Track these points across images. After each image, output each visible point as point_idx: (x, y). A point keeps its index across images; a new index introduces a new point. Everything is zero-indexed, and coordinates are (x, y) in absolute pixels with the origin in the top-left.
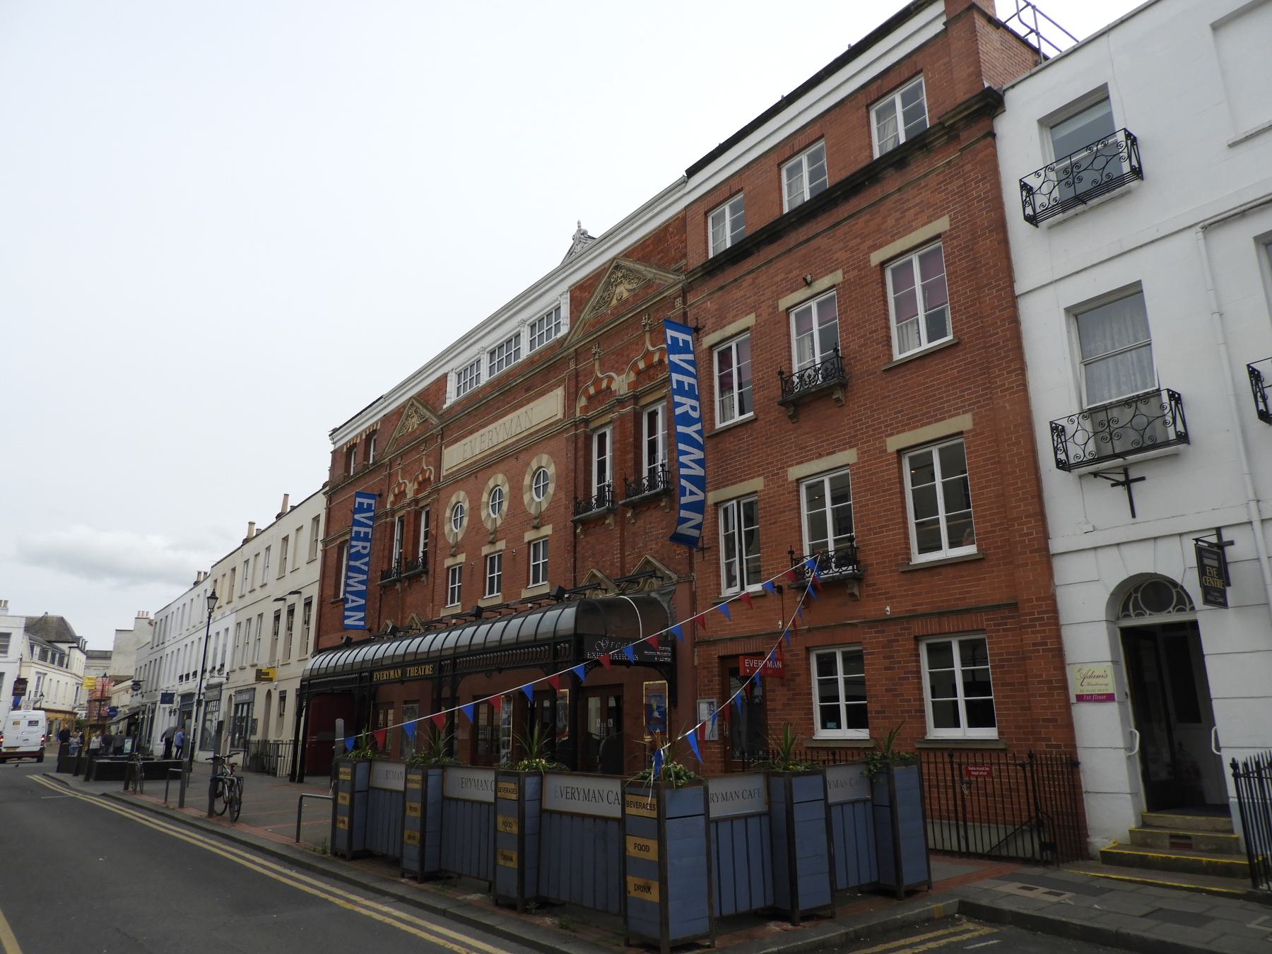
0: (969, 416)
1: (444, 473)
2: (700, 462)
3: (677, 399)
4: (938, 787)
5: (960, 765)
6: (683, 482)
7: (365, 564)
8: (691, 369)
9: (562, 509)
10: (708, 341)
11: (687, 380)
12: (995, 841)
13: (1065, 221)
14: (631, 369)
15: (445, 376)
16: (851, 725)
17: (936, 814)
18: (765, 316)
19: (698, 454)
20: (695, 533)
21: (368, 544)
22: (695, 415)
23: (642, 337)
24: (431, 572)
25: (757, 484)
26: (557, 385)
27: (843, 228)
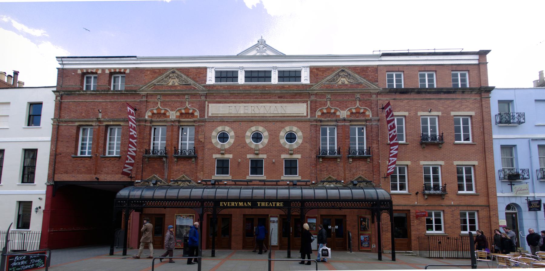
3: (131, 129)
6: (128, 156)
11: (133, 125)
13: (506, 126)
14: (349, 110)
18: (412, 114)
19: (135, 149)
20: (130, 172)
22: (135, 136)
24: (200, 157)
25: (408, 163)
27: (442, 101)
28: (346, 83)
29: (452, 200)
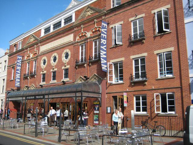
0: (173, 48)
1: (40, 52)
2: (104, 54)
4: (164, 123)
5: (171, 119)
7: (105, 48)
8: (106, 33)
9: (72, 62)
10: (111, 26)
12: (176, 133)
15: (61, 19)
16: (143, 111)
17: (167, 129)
19: (105, 53)
21: (105, 41)
23: (94, 24)
26: (71, 33)
28: (90, 14)
29: (153, 85)
